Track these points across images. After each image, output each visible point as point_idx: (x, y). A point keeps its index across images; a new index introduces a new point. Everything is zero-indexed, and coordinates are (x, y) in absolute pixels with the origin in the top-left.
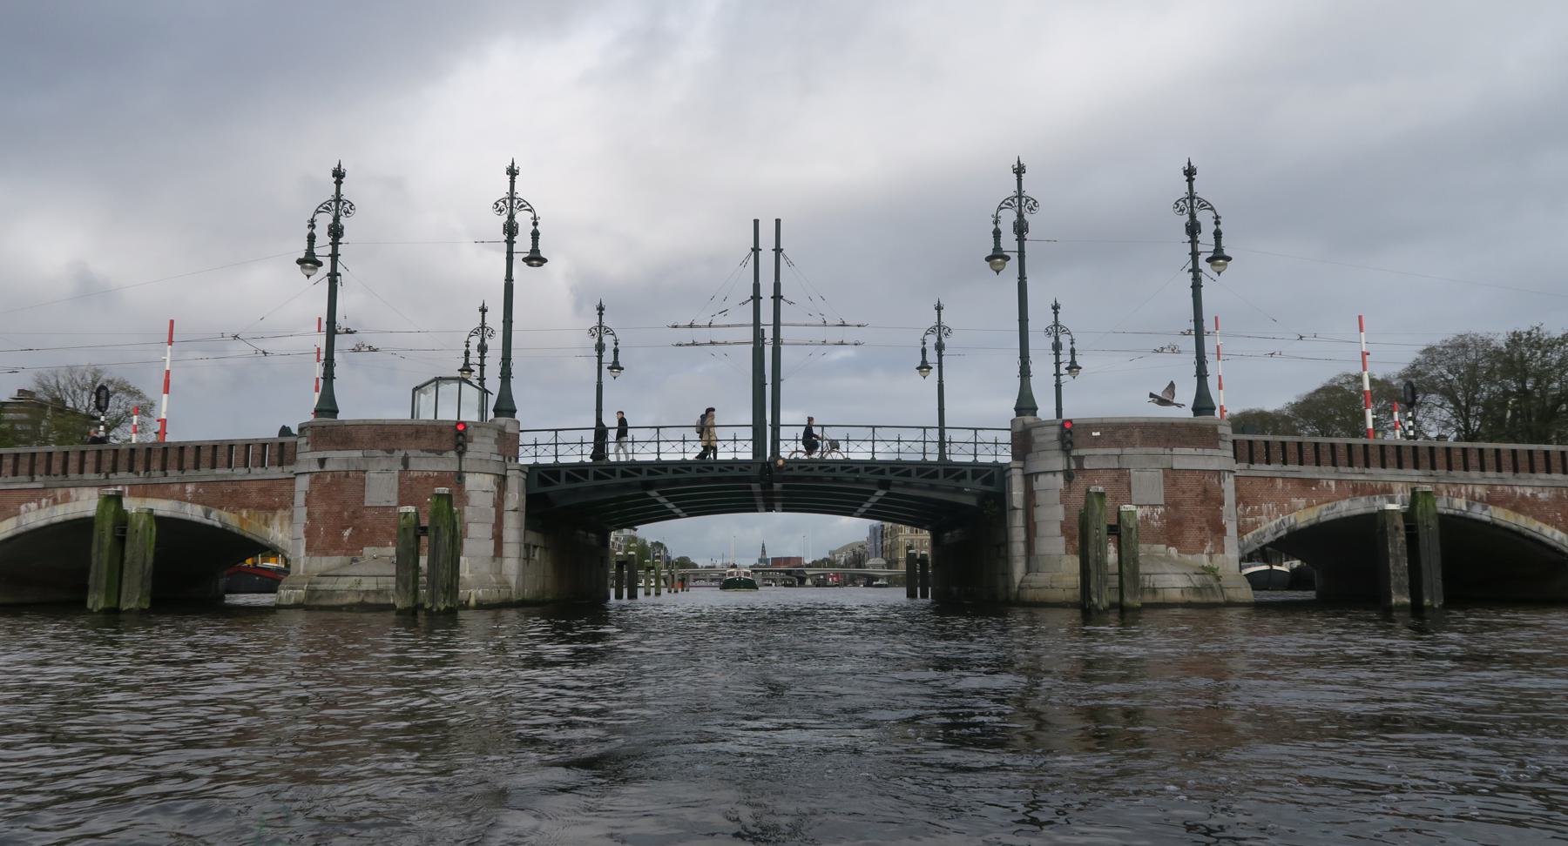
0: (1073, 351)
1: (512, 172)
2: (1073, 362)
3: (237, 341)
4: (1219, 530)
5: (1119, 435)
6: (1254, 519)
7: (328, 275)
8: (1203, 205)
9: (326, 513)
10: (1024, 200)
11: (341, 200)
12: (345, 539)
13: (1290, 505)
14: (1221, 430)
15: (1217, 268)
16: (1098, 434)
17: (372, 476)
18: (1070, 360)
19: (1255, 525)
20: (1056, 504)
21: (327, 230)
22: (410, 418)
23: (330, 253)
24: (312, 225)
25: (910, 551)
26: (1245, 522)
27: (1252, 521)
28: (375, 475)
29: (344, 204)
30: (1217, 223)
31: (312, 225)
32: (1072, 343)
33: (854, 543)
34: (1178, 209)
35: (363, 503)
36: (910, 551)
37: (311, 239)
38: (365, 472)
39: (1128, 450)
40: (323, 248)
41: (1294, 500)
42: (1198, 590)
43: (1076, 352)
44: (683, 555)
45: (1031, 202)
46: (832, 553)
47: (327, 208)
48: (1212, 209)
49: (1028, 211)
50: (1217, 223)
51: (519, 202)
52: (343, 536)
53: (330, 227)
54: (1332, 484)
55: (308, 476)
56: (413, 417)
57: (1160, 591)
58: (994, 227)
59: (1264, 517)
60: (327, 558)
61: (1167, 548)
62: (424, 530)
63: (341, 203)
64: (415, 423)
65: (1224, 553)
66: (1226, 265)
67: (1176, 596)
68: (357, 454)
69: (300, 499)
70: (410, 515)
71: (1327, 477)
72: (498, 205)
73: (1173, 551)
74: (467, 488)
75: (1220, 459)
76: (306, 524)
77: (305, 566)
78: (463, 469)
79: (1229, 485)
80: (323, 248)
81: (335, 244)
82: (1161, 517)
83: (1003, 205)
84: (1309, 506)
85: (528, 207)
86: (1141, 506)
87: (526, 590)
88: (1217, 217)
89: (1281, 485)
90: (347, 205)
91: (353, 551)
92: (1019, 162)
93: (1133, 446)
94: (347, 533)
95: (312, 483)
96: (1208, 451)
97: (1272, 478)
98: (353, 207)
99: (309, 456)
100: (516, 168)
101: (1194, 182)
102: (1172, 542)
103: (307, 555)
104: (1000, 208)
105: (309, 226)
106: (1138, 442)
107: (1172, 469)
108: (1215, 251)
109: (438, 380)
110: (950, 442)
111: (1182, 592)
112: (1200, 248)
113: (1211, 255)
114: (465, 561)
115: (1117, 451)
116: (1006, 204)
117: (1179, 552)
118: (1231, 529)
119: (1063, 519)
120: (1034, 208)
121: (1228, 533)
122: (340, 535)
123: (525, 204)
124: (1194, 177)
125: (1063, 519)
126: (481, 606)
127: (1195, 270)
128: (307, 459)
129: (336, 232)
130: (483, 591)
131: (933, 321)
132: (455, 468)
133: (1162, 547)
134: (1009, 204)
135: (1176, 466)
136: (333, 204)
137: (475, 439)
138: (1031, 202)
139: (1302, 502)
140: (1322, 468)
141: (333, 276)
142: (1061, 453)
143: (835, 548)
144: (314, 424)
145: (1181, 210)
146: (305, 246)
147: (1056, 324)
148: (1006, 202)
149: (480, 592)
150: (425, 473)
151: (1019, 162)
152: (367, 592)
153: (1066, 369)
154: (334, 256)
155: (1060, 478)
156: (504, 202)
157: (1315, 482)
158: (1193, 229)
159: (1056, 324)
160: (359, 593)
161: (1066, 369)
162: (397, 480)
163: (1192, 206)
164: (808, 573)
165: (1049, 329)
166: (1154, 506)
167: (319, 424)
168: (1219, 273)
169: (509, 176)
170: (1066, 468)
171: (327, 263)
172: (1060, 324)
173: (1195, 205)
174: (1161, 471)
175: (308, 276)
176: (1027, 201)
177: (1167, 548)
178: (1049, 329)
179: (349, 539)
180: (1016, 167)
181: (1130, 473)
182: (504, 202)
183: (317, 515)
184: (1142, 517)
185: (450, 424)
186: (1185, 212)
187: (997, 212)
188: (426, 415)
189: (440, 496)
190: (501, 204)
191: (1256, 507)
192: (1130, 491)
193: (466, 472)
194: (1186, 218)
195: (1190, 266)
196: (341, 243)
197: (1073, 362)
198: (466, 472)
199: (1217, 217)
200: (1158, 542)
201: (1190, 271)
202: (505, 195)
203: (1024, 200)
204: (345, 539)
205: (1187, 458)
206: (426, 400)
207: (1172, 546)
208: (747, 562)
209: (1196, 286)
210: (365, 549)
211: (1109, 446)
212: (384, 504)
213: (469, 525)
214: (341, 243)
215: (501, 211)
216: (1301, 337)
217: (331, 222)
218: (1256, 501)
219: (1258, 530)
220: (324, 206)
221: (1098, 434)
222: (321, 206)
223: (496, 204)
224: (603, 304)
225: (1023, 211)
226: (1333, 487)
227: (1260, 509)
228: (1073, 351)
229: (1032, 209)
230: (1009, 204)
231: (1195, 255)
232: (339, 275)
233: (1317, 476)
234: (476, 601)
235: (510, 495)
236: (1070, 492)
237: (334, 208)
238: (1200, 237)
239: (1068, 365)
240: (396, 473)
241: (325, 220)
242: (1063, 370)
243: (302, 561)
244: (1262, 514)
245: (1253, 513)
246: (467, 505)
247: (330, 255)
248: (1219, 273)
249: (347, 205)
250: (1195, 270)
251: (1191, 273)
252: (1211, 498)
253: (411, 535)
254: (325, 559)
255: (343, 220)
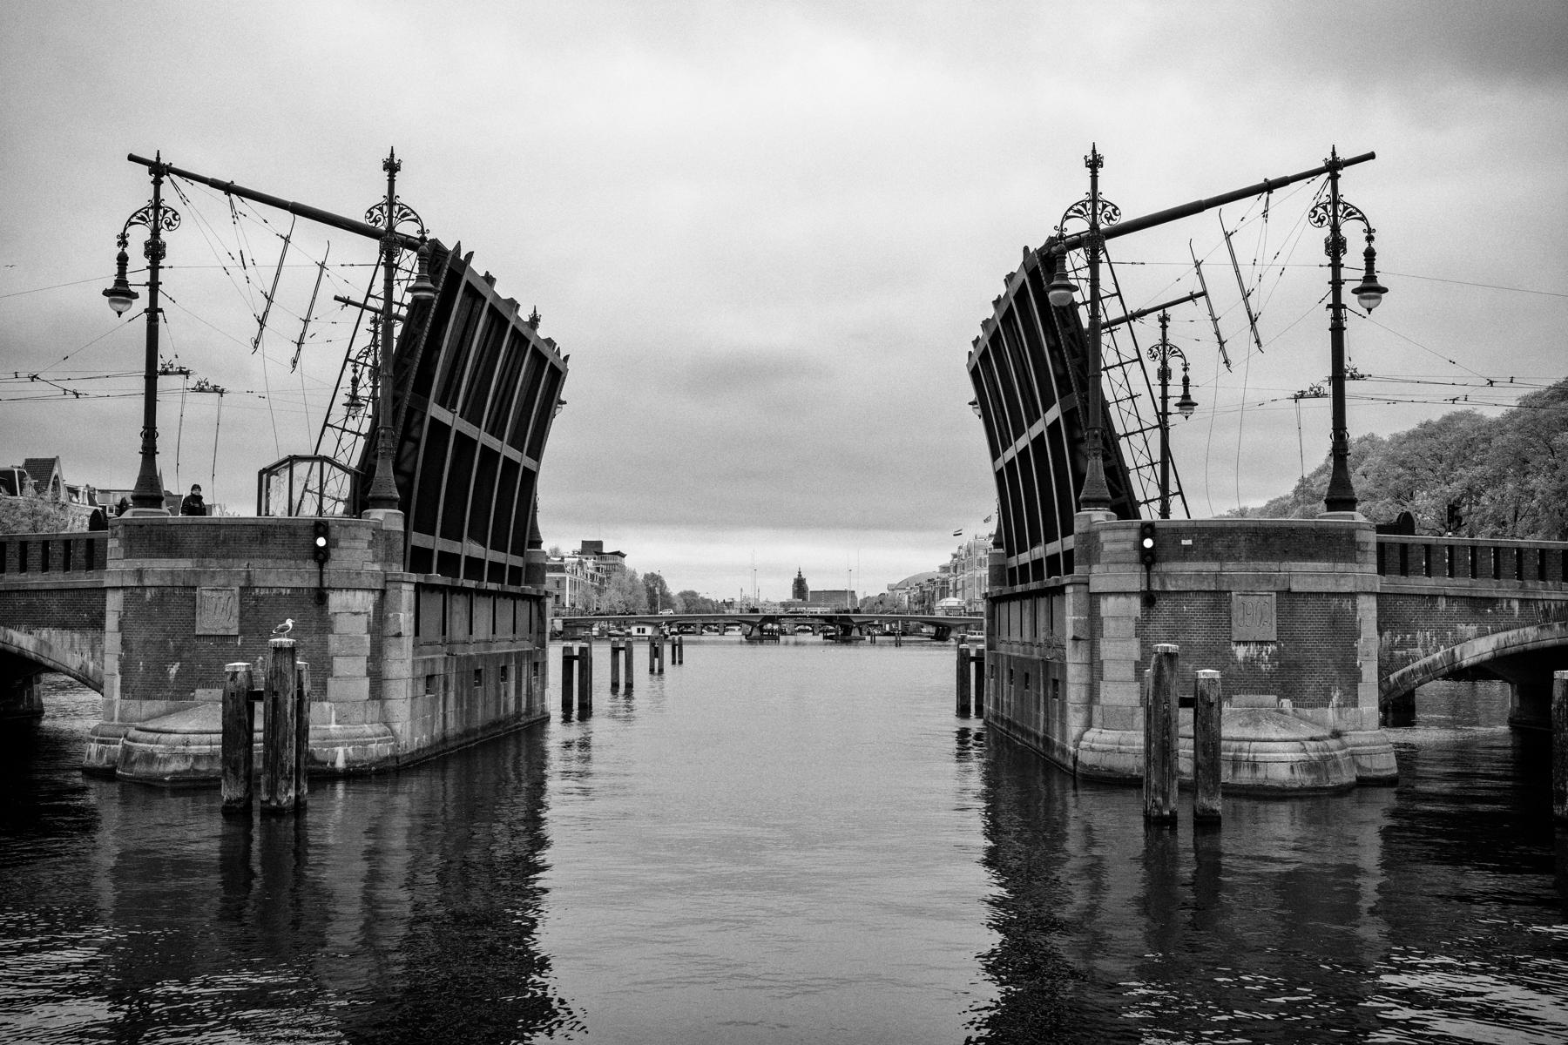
0: (1186, 380)
1: (392, 167)
2: (1186, 396)
3: (37, 383)
4: (1353, 676)
5: (1218, 546)
6: (1404, 652)
7: (146, 311)
8: (1350, 214)
9: (146, 642)
10: (1100, 205)
11: (161, 207)
12: (171, 678)
13: (1455, 632)
14: (1361, 536)
15: (1366, 302)
16: (1189, 542)
17: (204, 593)
18: (1182, 393)
19: (1405, 661)
20: (1130, 638)
21: (142, 249)
22: (254, 514)
23: (148, 280)
24: (123, 241)
25: (961, 646)
26: (1392, 655)
27: (1402, 655)
28: (209, 594)
29: (165, 212)
30: (1370, 239)
31: (123, 241)
32: (1185, 370)
33: (921, 575)
34: (1316, 219)
35: (194, 630)
36: (961, 646)
37: (123, 260)
38: (194, 588)
39: (1230, 565)
40: (138, 275)
41: (1461, 627)
42: (1311, 767)
43: (1190, 383)
44: (688, 589)
45: (1110, 209)
46: (892, 588)
47: (142, 218)
48: (1363, 219)
49: (1105, 221)
50: (1370, 239)
51: (401, 209)
52: (168, 674)
53: (147, 244)
54: (1516, 604)
55: (121, 592)
56: (259, 513)
57: (1261, 766)
58: (120, 250)
59: (1419, 650)
60: (148, 702)
61: (1279, 700)
62: (259, 696)
63: (162, 211)
64: (261, 522)
65: (1355, 705)
66: (1380, 298)
67: (1280, 774)
68: (184, 564)
69: (111, 621)
70: (239, 675)
71: (1508, 595)
72: (372, 214)
73: (1287, 704)
74: (331, 610)
75: (1364, 574)
76: (120, 656)
77: (121, 711)
78: (326, 585)
79: (1367, 610)
80: (138, 275)
81: (154, 268)
82: (1273, 657)
83: (1071, 213)
84: (1482, 634)
85: (413, 216)
86: (1246, 643)
87: (416, 739)
88: (1370, 231)
89: (1444, 606)
90: (170, 215)
91: (181, 694)
92: (1094, 151)
93: (1237, 559)
94: (173, 670)
95: (126, 601)
96: (1341, 566)
97: (1433, 597)
98: (177, 217)
99: (122, 565)
100: (396, 162)
101: (1339, 181)
102: (1285, 692)
103: (123, 697)
104: (1066, 217)
105: (119, 244)
106: (1243, 554)
107: (1289, 591)
108: (1366, 279)
109: (292, 460)
110: (1111, 331)
111: (1292, 768)
112: (1344, 274)
113: (1358, 284)
114: (330, 708)
115: (1215, 566)
116: (1075, 211)
117: (1294, 706)
118: (1370, 672)
119: (1139, 659)
120: (1114, 217)
121: (1364, 677)
122: (165, 673)
123: (409, 212)
124: (1339, 172)
125: (1139, 659)
126: (356, 775)
127: (1337, 306)
128: (118, 567)
129: (155, 251)
130: (353, 749)
131: (1082, 190)
132: (314, 583)
133: (1272, 699)
134: (1079, 211)
135: (1295, 588)
136: (151, 212)
137: (341, 544)
138: (1110, 209)
139: (1472, 629)
140: (1503, 582)
141: (153, 312)
142: (1139, 568)
143: (896, 581)
144: (128, 523)
145: (1319, 220)
146: (114, 269)
147: (1164, 342)
148: (1075, 208)
149: (350, 749)
150: (275, 591)
151: (1094, 151)
152: (197, 758)
153: (1176, 405)
154: (154, 285)
155: (1136, 603)
156: (381, 209)
157: (1492, 601)
158: (1336, 247)
159: (1164, 342)
160: (186, 757)
161: (1176, 405)
162: (237, 599)
163: (1335, 215)
164: (855, 621)
165: (1154, 350)
166: (1262, 643)
167: (136, 523)
168: (1369, 310)
169: (387, 173)
170: (1144, 588)
171: (144, 293)
172: (1170, 342)
173: (1339, 213)
174: (1274, 594)
175: (120, 313)
176: (1105, 206)
177: (1279, 700)
178: (1154, 350)
179: (176, 678)
180: (1091, 158)
181: (1231, 596)
182: (381, 209)
183: (134, 646)
184: (1246, 658)
185: (307, 523)
186: (1325, 222)
187: (125, 229)
188: (278, 508)
189: (279, 650)
190: (376, 212)
191: (1408, 636)
192: (1230, 622)
193: (329, 588)
194: (1326, 231)
195: (1330, 300)
196: (162, 267)
197: (1186, 396)
198: (329, 588)
199: (1370, 231)
200: (1266, 692)
201: (1329, 306)
202: (382, 200)
203: (1100, 205)
204: (171, 678)
205: (1307, 575)
206: (279, 484)
207: (1286, 697)
208: (775, 593)
209: (1337, 330)
210: (198, 691)
211: (1204, 559)
212: (221, 632)
213: (335, 658)
214: (162, 267)
215: (1321, 221)
216: (1491, 382)
217: (148, 237)
218: (1408, 628)
219: (1410, 668)
220: (139, 215)
221: (1189, 542)
222: (134, 215)
223: (369, 211)
224: (538, 313)
225: (1098, 221)
226: (1517, 609)
227: (1414, 638)
228: (1186, 380)
229: (171, 224)
230: (1079, 211)
231: (1337, 284)
232: (161, 310)
233: (1496, 595)
234: (346, 761)
235: (391, 615)
236: (1148, 621)
237: (152, 218)
238: (1344, 259)
239: (1179, 400)
240: (237, 590)
241: (140, 235)
242: (1348, 297)
243: (117, 705)
244: (1415, 646)
245: (1403, 645)
246: (332, 633)
247: (147, 284)
248: (1369, 310)
249: (170, 215)
250: (1337, 306)
251: (1331, 310)
252: (1343, 629)
253: (242, 702)
254: (147, 703)
255: (164, 235)
